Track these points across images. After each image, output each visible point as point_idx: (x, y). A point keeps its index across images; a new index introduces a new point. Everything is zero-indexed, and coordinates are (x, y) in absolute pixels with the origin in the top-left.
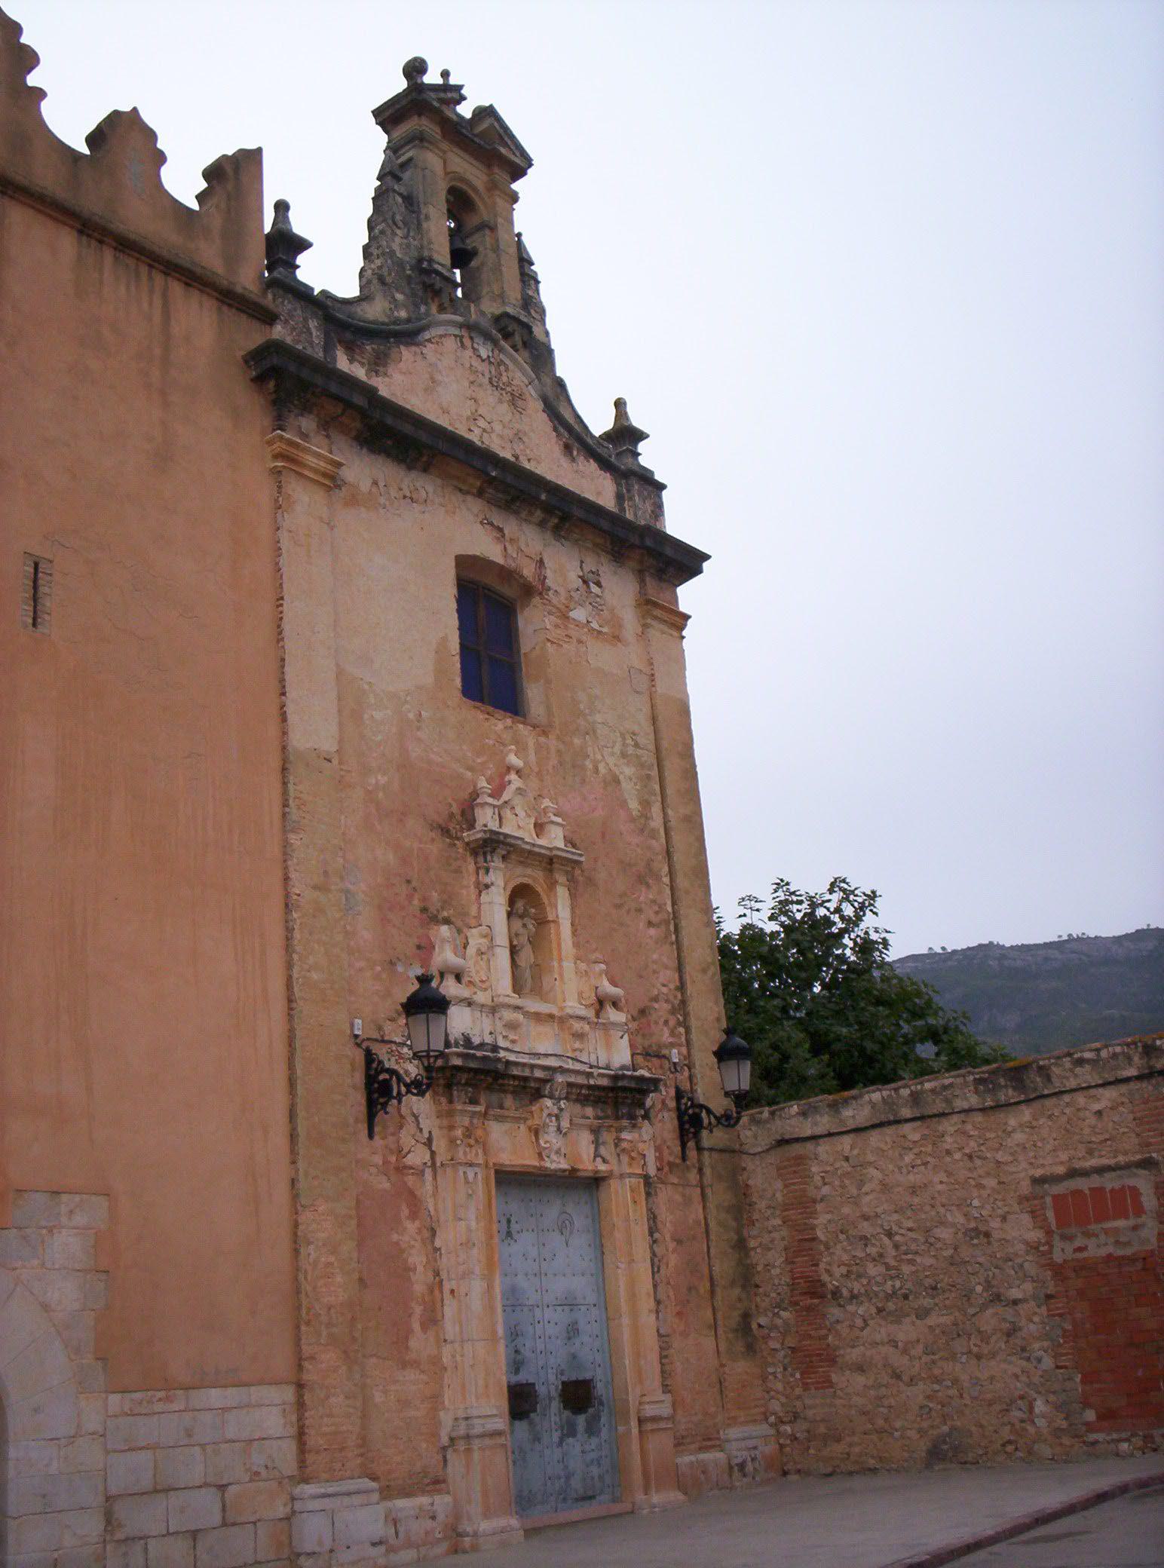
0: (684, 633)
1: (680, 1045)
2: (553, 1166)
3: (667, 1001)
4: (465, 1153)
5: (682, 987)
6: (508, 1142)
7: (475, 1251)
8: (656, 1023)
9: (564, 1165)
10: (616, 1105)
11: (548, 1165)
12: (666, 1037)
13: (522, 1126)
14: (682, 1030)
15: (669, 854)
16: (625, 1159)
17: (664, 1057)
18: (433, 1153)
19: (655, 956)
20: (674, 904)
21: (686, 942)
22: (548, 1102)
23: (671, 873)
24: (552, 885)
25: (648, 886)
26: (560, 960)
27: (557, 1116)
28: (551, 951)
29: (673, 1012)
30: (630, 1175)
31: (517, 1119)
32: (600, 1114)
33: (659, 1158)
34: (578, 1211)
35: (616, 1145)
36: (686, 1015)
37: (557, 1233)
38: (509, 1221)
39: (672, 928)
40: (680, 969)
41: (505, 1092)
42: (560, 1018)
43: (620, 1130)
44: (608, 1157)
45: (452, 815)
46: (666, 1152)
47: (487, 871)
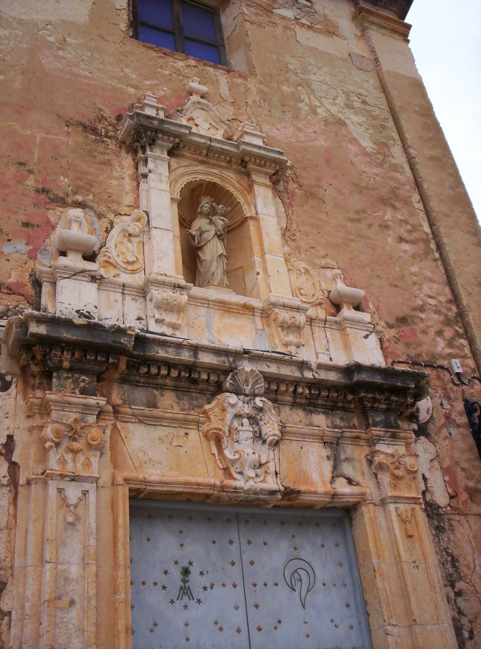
0: (409, 38)
1: (465, 357)
2: (247, 486)
3: (438, 312)
4: (63, 462)
5: (456, 299)
6: (163, 450)
7: (74, 614)
8: (424, 332)
9: (272, 484)
10: (364, 413)
11: (240, 483)
12: (441, 346)
13: (194, 435)
14: (464, 342)
15: (418, 185)
16: (385, 478)
17: (442, 367)
18: (14, 467)
19: (414, 269)
20: (431, 225)
21: (452, 257)
22: (233, 399)
23: (423, 199)
24: (250, 188)
25: (395, 208)
26: (263, 253)
27: (253, 420)
28: (251, 246)
29: (448, 322)
30: (396, 499)
31: (184, 423)
32: (338, 422)
33: (452, 483)
34: (320, 555)
35: (370, 462)
36: (466, 326)
37: (283, 592)
38: (186, 572)
39: (433, 246)
40: (450, 282)
41: (162, 387)
42: (263, 311)
43: (371, 442)
44: (358, 478)
45: (101, 118)
46: (460, 475)
47: (146, 161)
